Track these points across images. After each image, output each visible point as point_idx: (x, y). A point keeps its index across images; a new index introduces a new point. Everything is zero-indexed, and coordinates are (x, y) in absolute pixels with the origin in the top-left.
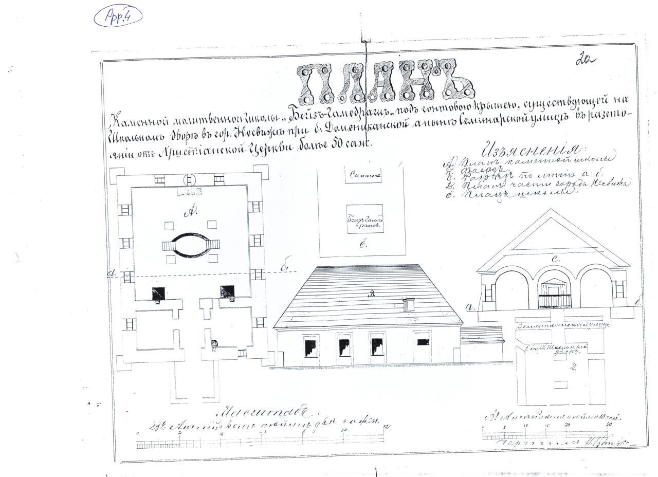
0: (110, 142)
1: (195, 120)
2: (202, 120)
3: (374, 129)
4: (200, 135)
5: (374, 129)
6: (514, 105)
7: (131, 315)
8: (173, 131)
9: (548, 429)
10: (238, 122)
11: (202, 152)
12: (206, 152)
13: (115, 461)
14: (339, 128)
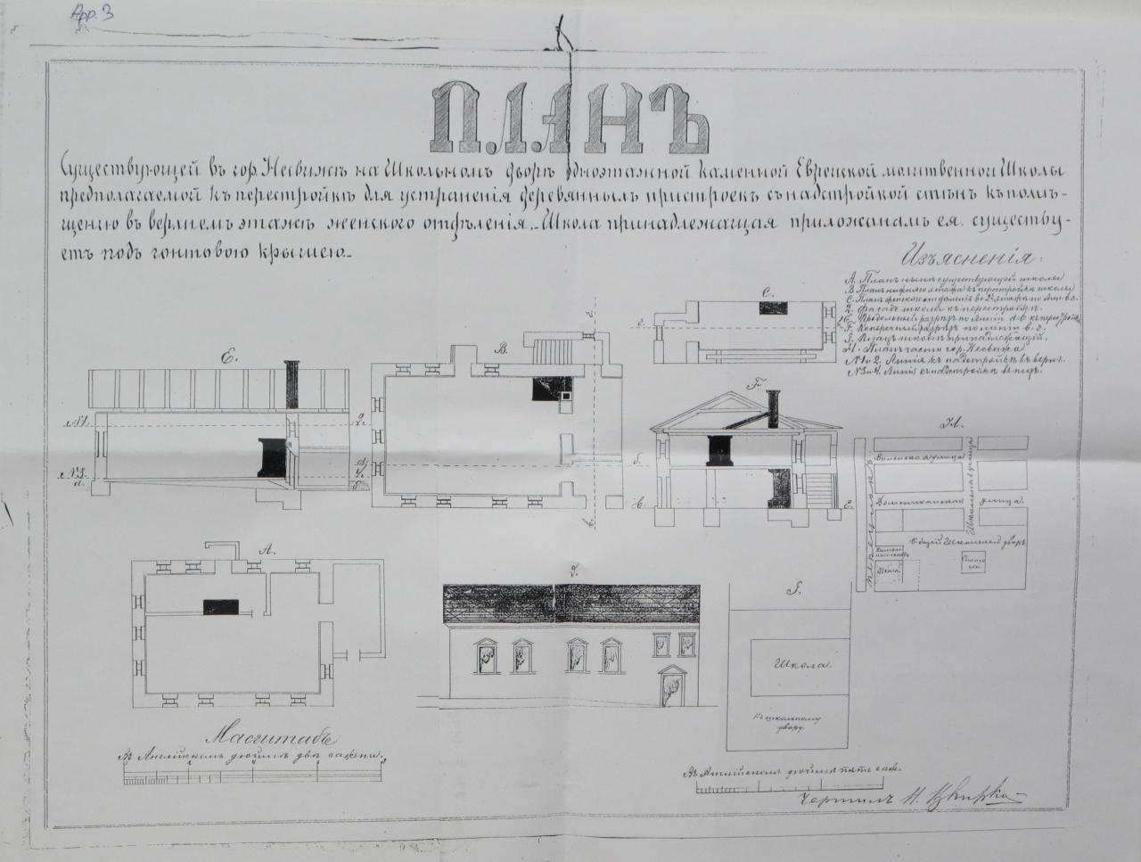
0: (1002, 175)
1: (918, 171)
2: (73, 253)
3: (659, 228)
4: (123, 223)
5: (659, 228)
6: (794, 222)
7: (314, 566)
8: (130, 243)
9: (650, 501)
10: (824, 198)
11: (123, 196)
12: (148, 196)
13: (46, 826)
14: (581, 223)
